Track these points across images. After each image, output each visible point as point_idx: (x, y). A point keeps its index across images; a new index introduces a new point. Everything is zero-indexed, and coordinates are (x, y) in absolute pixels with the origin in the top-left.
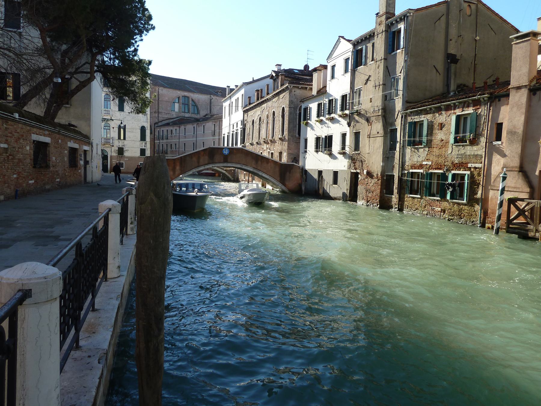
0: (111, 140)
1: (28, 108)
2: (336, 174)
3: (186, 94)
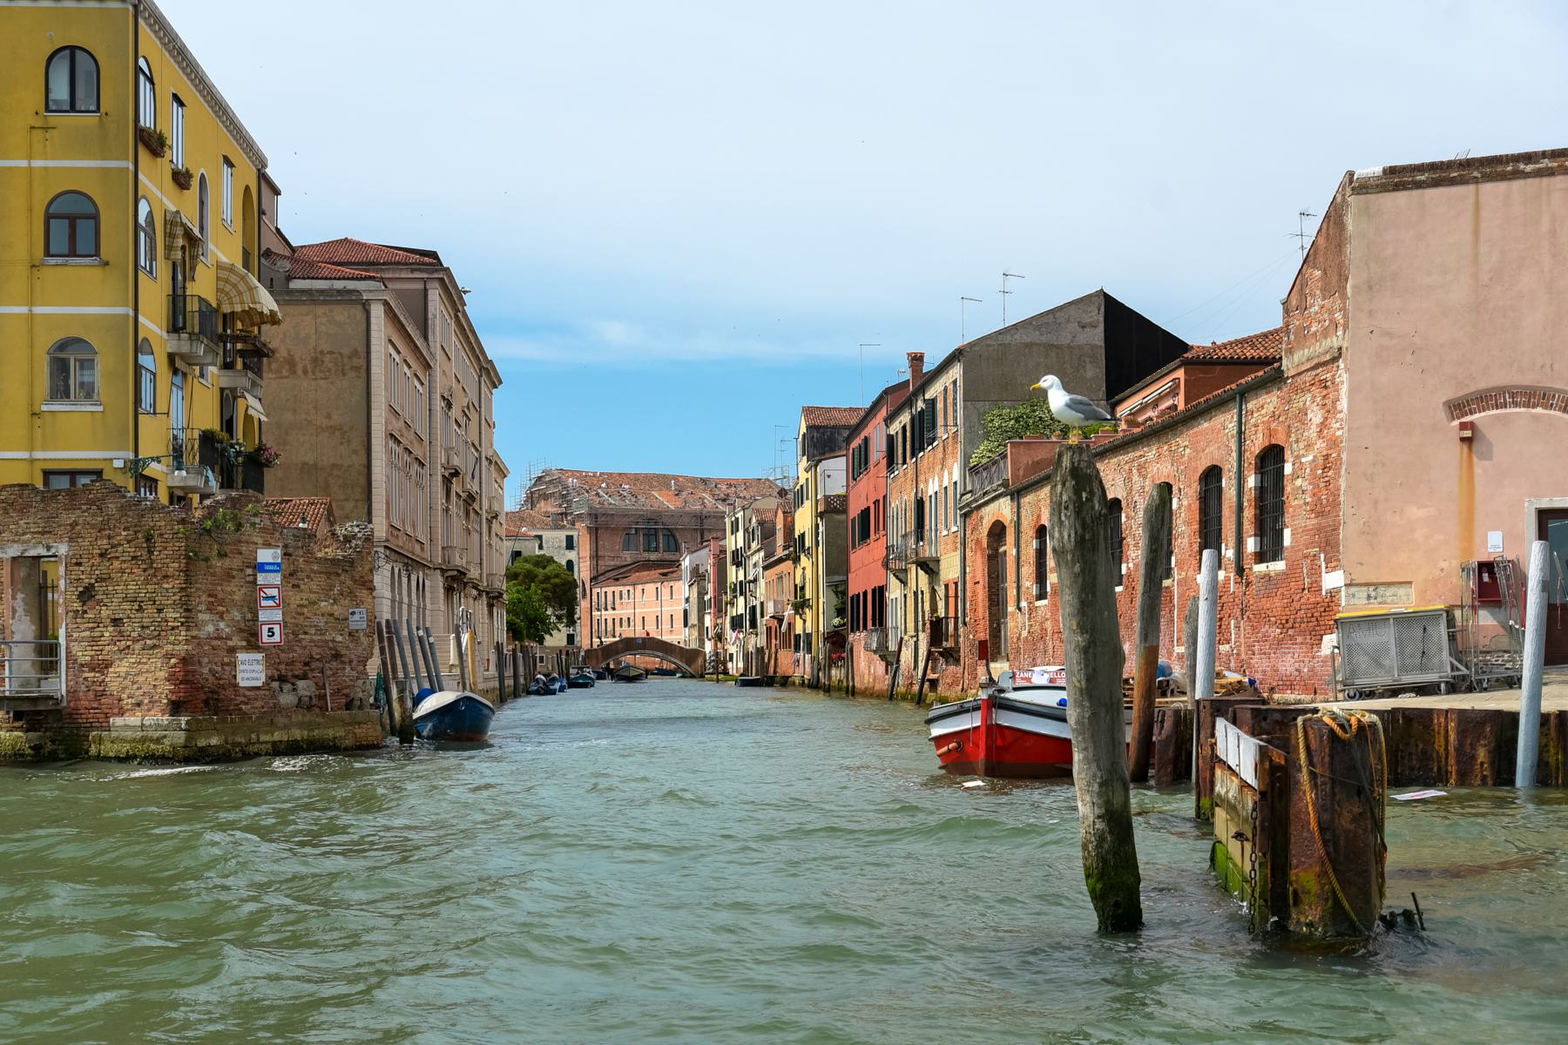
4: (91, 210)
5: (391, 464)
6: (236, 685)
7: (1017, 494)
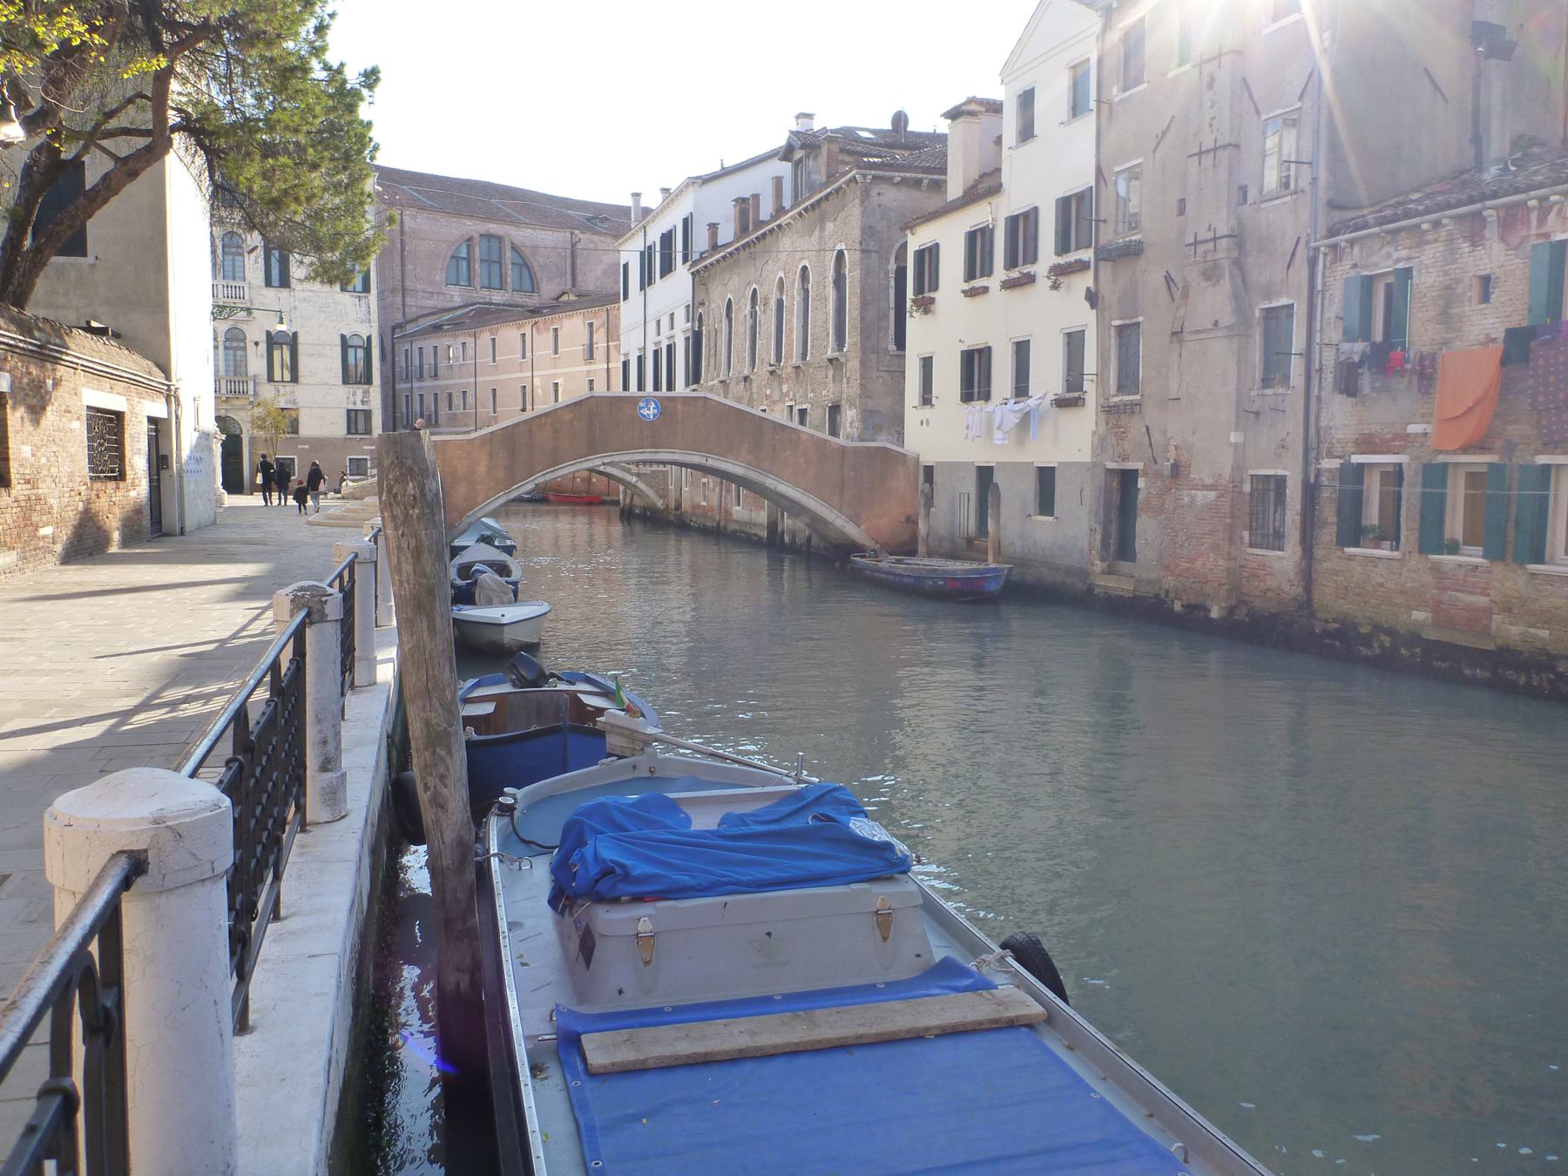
0: (251, 384)
2: (1046, 476)
3: (493, 228)
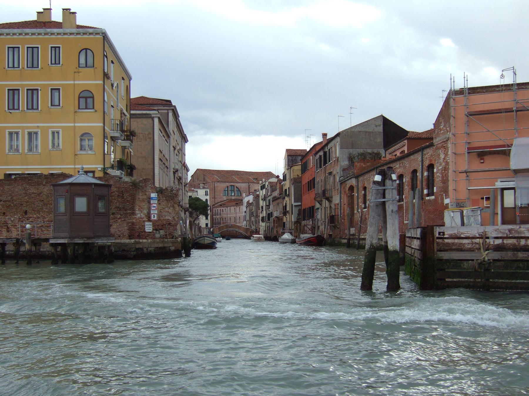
1: (43, 248)
4: (92, 96)
5: (160, 168)
6: (145, 232)
7: (357, 177)
